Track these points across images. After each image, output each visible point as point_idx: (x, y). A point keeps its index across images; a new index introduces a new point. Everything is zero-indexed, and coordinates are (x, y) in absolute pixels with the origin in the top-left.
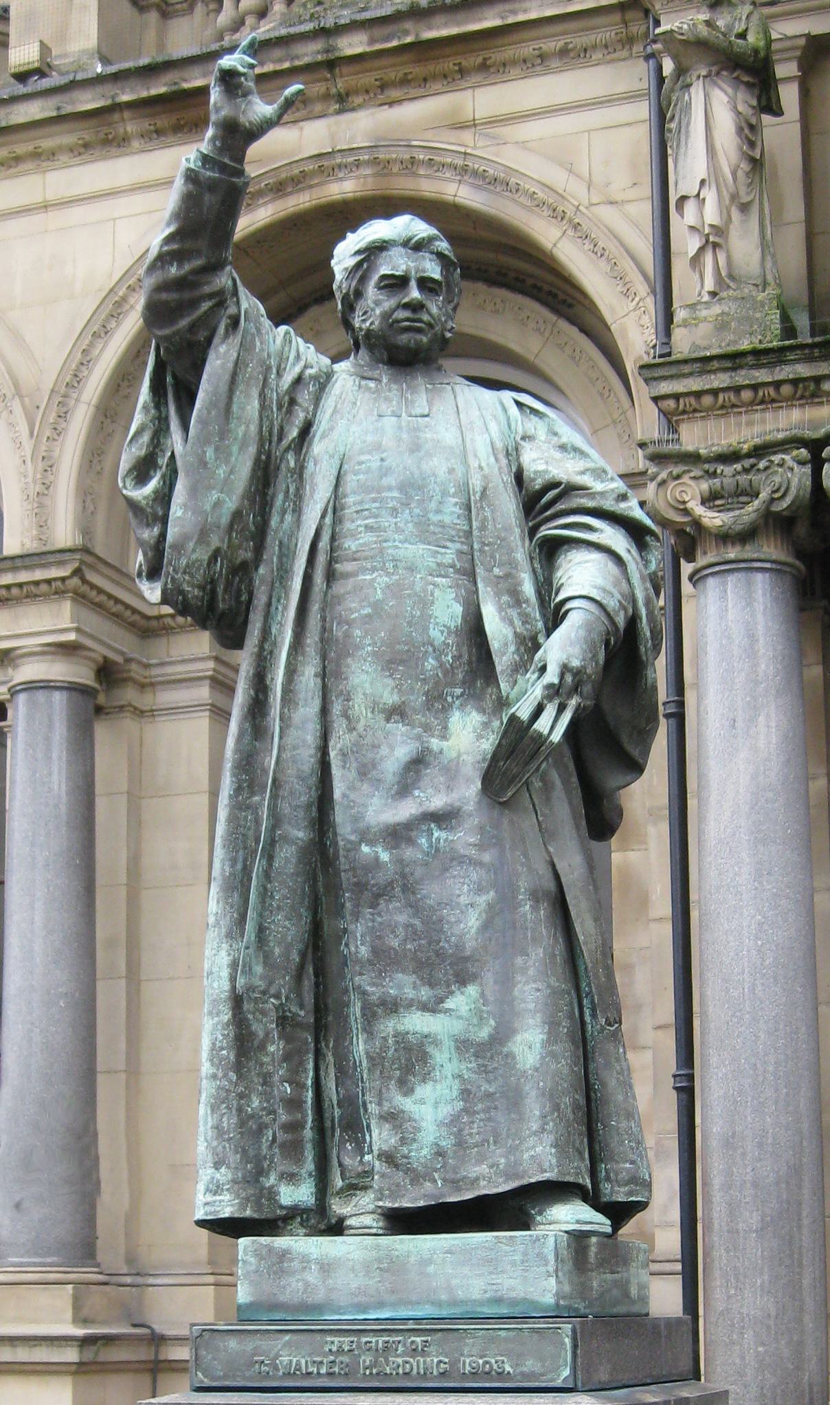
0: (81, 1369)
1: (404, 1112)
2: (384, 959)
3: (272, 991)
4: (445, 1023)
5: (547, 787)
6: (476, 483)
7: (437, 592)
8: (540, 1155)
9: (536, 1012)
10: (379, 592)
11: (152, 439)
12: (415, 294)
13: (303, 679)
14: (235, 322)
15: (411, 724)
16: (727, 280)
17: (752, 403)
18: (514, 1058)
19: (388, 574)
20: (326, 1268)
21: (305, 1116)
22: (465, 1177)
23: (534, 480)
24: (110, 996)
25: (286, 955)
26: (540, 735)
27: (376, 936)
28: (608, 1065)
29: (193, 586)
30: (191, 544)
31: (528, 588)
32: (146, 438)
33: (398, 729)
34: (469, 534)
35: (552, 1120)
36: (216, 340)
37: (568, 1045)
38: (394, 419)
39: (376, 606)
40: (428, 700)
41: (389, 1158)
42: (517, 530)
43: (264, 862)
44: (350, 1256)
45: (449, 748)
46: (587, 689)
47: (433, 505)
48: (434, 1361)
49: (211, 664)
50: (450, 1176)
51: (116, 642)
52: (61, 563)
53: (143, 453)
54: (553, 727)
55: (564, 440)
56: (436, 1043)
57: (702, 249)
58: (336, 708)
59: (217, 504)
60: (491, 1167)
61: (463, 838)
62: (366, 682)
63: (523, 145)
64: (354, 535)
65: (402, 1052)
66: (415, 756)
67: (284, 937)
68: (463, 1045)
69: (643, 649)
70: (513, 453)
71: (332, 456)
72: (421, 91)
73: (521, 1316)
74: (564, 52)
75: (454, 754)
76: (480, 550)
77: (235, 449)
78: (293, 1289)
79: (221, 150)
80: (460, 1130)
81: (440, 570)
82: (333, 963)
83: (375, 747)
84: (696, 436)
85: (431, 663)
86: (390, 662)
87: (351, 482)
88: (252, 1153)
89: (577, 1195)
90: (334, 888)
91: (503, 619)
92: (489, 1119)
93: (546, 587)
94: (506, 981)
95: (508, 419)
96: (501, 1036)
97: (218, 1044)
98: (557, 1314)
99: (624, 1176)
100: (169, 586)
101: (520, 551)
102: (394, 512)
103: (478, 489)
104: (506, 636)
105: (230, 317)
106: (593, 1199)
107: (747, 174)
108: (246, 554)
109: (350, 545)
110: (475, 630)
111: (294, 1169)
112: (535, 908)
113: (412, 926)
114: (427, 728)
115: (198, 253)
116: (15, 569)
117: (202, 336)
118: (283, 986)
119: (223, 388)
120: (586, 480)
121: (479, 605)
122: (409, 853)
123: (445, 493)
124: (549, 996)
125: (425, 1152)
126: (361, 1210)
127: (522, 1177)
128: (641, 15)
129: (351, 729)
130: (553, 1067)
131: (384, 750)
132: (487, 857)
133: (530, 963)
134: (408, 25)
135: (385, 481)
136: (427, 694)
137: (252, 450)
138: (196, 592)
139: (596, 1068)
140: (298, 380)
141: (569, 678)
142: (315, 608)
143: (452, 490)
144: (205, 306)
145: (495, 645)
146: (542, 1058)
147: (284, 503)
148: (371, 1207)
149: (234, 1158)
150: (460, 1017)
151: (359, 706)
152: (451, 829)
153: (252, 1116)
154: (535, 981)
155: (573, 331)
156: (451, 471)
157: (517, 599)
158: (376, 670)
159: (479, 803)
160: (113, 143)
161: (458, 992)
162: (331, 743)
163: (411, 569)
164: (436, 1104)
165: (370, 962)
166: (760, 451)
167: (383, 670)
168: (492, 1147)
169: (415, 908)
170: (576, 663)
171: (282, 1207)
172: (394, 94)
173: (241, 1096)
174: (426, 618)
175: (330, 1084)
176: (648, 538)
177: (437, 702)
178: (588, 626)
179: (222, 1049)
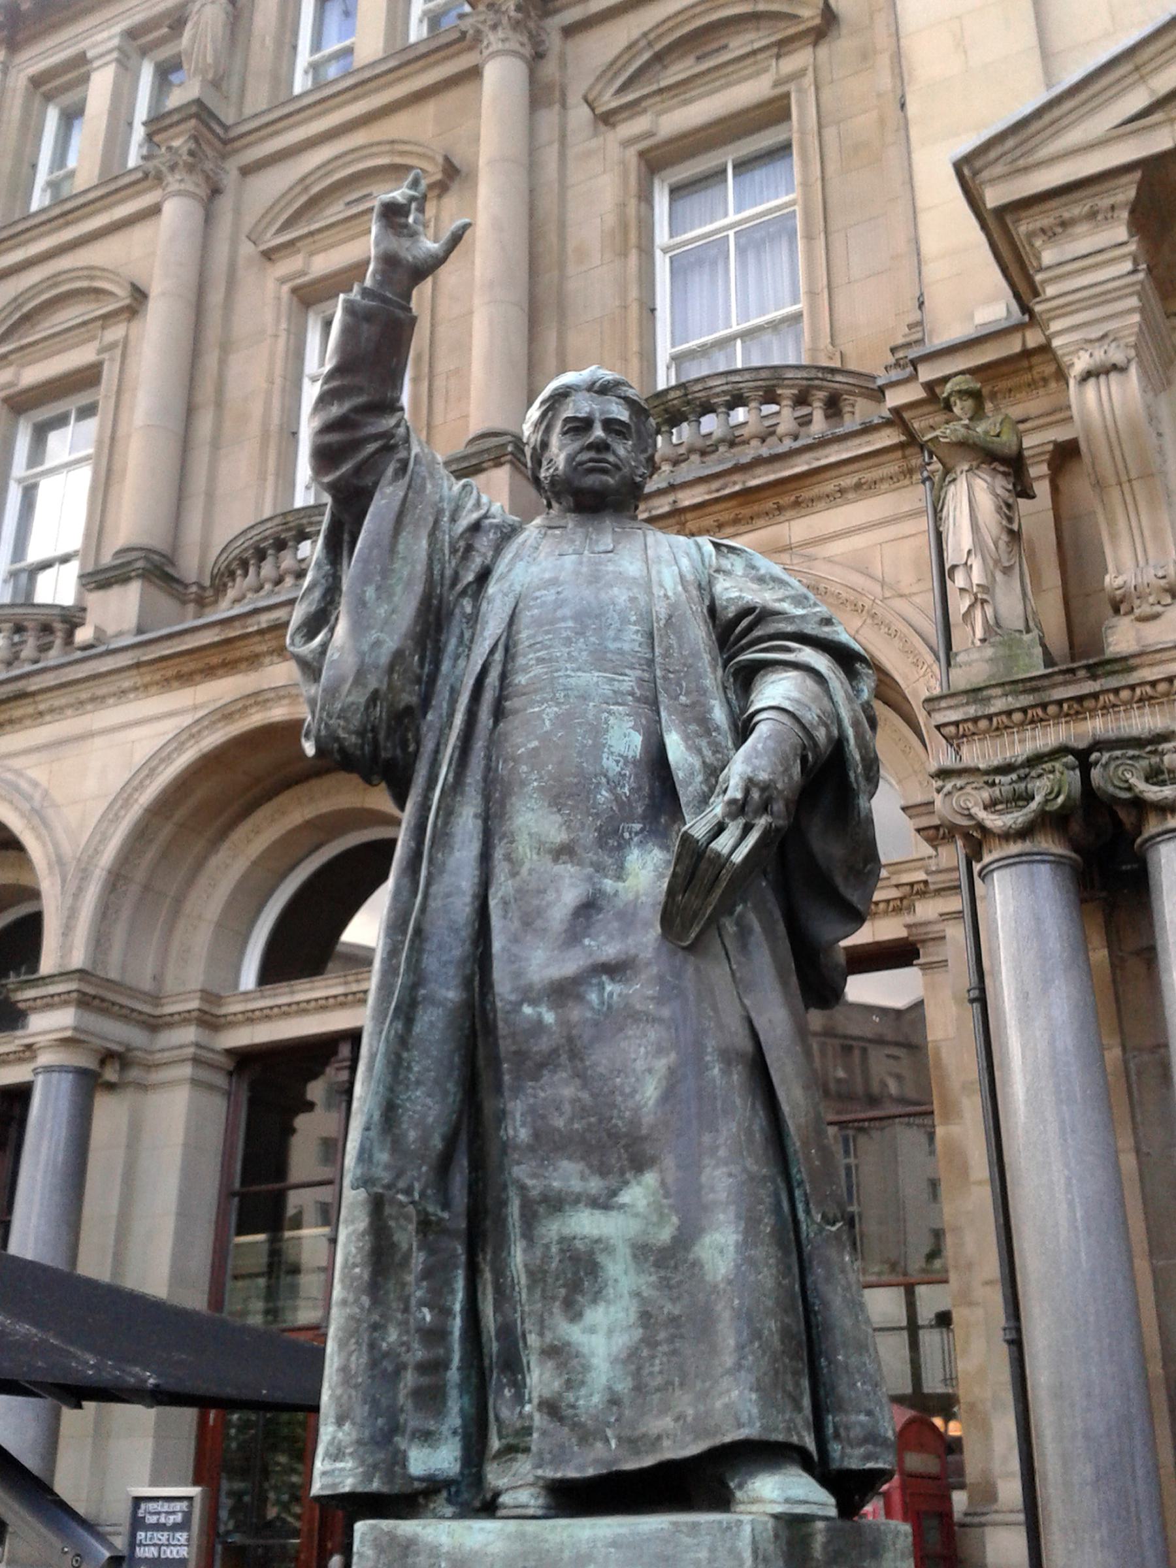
1: (569, 1344)
2: (548, 1144)
3: (402, 1184)
4: (616, 1223)
5: (744, 931)
6: (661, 609)
7: (612, 721)
8: (732, 1402)
9: (728, 1204)
10: (547, 723)
11: (324, 596)
13: (461, 821)
15: (580, 863)
16: (994, 628)
17: (1022, 724)
18: (702, 1267)
19: (558, 704)
21: (449, 1351)
22: (644, 1435)
23: (726, 608)
25: (425, 1139)
26: (719, 855)
27: (535, 1114)
28: (829, 1278)
29: (350, 733)
30: (347, 686)
32: (317, 594)
33: (567, 870)
34: (651, 662)
35: (753, 1353)
36: (383, 482)
37: (773, 1250)
38: (574, 557)
39: (545, 738)
40: (600, 838)
41: (551, 1408)
42: (707, 657)
43: (399, 1025)
44: (490, 1549)
45: (626, 890)
46: (778, 806)
47: (611, 633)
50: (627, 1432)
53: (313, 608)
55: (762, 571)
56: (609, 1250)
57: (972, 606)
58: (498, 854)
59: (377, 644)
60: (677, 1419)
62: (533, 822)
63: (829, 560)
64: (525, 669)
65: (568, 1263)
66: (585, 900)
67: (424, 1116)
68: (642, 1252)
69: (852, 775)
70: (705, 588)
71: (506, 595)
72: (749, 527)
74: (858, 486)
75: (631, 896)
76: (665, 678)
77: (399, 589)
79: (381, 284)
80: (639, 1369)
81: (617, 698)
83: (541, 892)
84: (976, 754)
85: (604, 795)
86: (558, 796)
87: (525, 617)
88: (384, 1402)
89: (792, 1461)
91: (688, 748)
92: (674, 1352)
94: (691, 1167)
95: (702, 555)
96: (685, 1239)
97: (351, 1260)
99: (856, 1432)
100: (323, 733)
101: (711, 677)
102: (568, 642)
103: (663, 616)
104: (692, 765)
105: (399, 461)
107: (1007, 544)
108: (409, 698)
109: (521, 679)
110: (657, 761)
111: (431, 1425)
112: (726, 1072)
113: (579, 1100)
114: (599, 868)
115: (360, 390)
117: (368, 481)
118: (418, 1179)
119: (388, 525)
120: (786, 606)
121: (662, 736)
122: (576, 1013)
123: (625, 621)
124: (744, 1183)
125: (596, 1399)
127: (715, 1435)
128: (917, 450)
129: (514, 874)
130: (752, 1278)
131: (551, 896)
132: (666, 1012)
133: (721, 1140)
134: (735, 478)
135: (559, 614)
136: (599, 830)
137: (419, 588)
138: (353, 739)
139: (815, 1283)
140: (476, 527)
141: (755, 795)
142: (479, 745)
143: (634, 618)
144: (371, 447)
145: (679, 775)
146: (738, 1267)
147: (457, 647)
148: (530, 1478)
149: (361, 1411)
150: (636, 1215)
151: (524, 848)
152: (627, 981)
153: (386, 1355)
154: (726, 1164)
156: (633, 600)
158: (541, 807)
159: (658, 950)
161: (634, 1183)
162: (492, 891)
163: (584, 697)
164: (610, 1332)
165: (531, 1148)
166: (1035, 760)
167: (550, 806)
168: (678, 1393)
169: (582, 1077)
170: (763, 776)
171: (413, 1479)
173: (375, 1327)
174: (598, 748)
175: (488, 1309)
176: (858, 665)
177: (611, 840)
179: (355, 1265)
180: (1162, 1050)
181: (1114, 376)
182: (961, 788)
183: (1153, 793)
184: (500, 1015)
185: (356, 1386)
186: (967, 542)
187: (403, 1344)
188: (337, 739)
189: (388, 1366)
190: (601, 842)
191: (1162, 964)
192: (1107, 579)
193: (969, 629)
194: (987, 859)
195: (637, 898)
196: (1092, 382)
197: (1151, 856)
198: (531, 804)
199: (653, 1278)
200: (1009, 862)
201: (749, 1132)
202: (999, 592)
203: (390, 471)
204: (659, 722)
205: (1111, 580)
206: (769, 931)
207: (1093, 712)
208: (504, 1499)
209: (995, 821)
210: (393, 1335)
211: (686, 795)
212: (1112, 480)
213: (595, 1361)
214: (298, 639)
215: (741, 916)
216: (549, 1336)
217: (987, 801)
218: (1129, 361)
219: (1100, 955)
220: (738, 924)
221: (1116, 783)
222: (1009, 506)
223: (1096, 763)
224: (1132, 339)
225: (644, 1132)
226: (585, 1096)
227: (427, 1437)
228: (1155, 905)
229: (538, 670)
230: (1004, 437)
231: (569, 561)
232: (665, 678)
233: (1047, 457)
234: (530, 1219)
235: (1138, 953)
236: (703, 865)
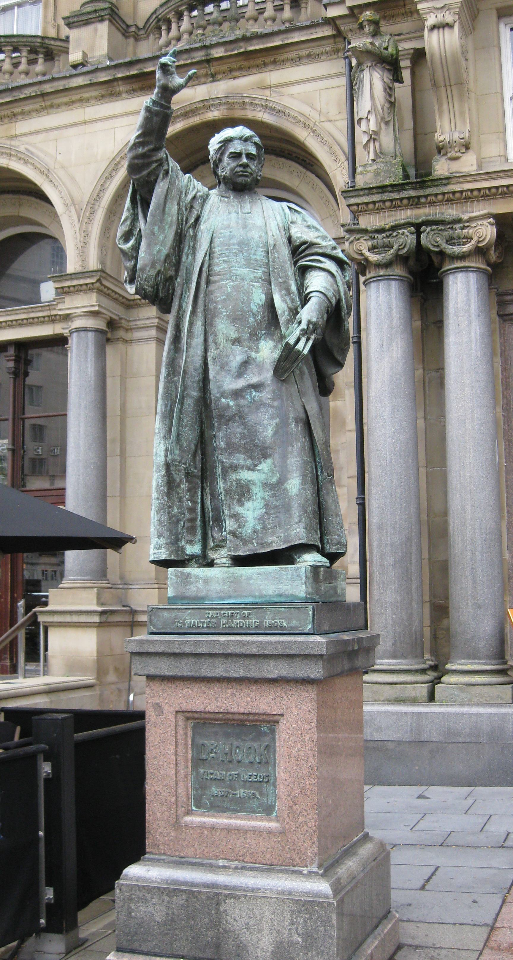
0: (100, 625)
2: (231, 448)
3: (183, 462)
4: (258, 475)
5: (302, 373)
6: (271, 242)
8: (299, 533)
11: (131, 223)
12: (244, 160)
13: (197, 327)
14: (167, 172)
15: (243, 346)
16: (379, 154)
17: (390, 207)
18: (287, 490)
19: (233, 281)
20: (206, 581)
21: (197, 515)
23: (296, 241)
24: (113, 464)
26: (299, 351)
28: (328, 493)
29: (149, 287)
30: (148, 268)
32: (128, 223)
34: (268, 264)
36: (159, 180)
39: (228, 295)
40: (250, 336)
41: (233, 533)
42: (289, 263)
43: (179, 406)
46: (319, 331)
47: (252, 252)
48: (253, 621)
51: (115, 311)
52: (92, 277)
53: (127, 229)
54: (304, 347)
55: (309, 223)
56: (254, 484)
57: (368, 141)
58: (211, 339)
59: (159, 251)
61: (265, 395)
62: (224, 328)
67: (188, 438)
68: (265, 485)
69: (343, 314)
71: (209, 230)
73: (290, 602)
74: (309, 56)
75: (261, 359)
76: (273, 271)
77: (167, 227)
78: (192, 590)
79: (161, 98)
80: (264, 522)
82: (209, 449)
83: (227, 356)
85: (251, 320)
86: (234, 319)
87: (217, 241)
88: (174, 531)
90: (210, 417)
91: (283, 301)
92: (277, 517)
93: (301, 287)
94: (284, 457)
95: (285, 214)
96: (282, 481)
98: (306, 601)
101: (290, 271)
102: (236, 254)
103: (272, 244)
105: (165, 170)
106: (321, 551)
107: (388, 108)
108: (171, 273)
109: (217, 269)
110: (270, 305)
112: (296, 426)
113: (243, 433)
114: (250, 348)
116: (72, 279)
120: (319, 241)
122: (242, 402)
125: (249, 531)
126: (221, 556)
128: (342, 40)
129: (217, 348)
130: (304, 494)
131: (231, 358)
132: (276, 404)
135: (232, 241)
136: (250, 333)
138: (150, 289)
140: (194, 198)
141: (311, 326)
144: (154, 165)
145: (279, 312)
146: (300, 490)
149: (167, 534)
150: (264, 473)
151: (220, 338)
152: (260, 391)
153: (174, 516)
156: (260, 237)
157: (289, 292)
159: (272, 380)
160: (114, 95)
162: (208, 354)
163: (243, 279)
165: (225, 449)
166: (394, 228)
169: (245, 426)
170: (314, 320)
172: (236, 74)
173: (170, 507)
174: (249, 300)
175: (208, 502)
176: (345, 266)
177: (254, 337)
178: (319, 304)
179: (161, 486)
180: (441, 371)
181: (447, 30)
182: (358, 239)
183: (450, 249)
184: (213, 402)
185: (164, 526)
187: (179, 512)
188: (144, 289)
189: (174, 519)
190: (250, 338)
191: (445, 333)
192: (436, 136)
193: (366, 153)
194: (368, 276)
195: (264, 360)
196: (436, 31)
197: (445, 280)
198: (224, 321)
199: (270, 493)
200: (379, 279)
201: (304, 446)
203: (161, 176)
204: (271, 289)
205: (438, 137)
206: (310, 371)
207: (424, 205)
208: (216, 561)
209: (373, 258)
211: (282, 319)
212: (443, 85)
213: (248, 519)
214: (121, 241)
215: (301, 367)
216: (232, 511)
217: (371, 247)
218: (455, 22)
220: (300, 370)
221: (433, 243)
222: (390, 88)
223: (424, 232)
224: (457, 10)
225: (267, 445)
226: (245, 432)
227: (191, 542)
228: (445, 304)
230: (390, 50)
231: (234, 215)
232: (273, 271)
233: (410, 56)
234: (225, 473)
235: (435, 323)
236: (293, 353)
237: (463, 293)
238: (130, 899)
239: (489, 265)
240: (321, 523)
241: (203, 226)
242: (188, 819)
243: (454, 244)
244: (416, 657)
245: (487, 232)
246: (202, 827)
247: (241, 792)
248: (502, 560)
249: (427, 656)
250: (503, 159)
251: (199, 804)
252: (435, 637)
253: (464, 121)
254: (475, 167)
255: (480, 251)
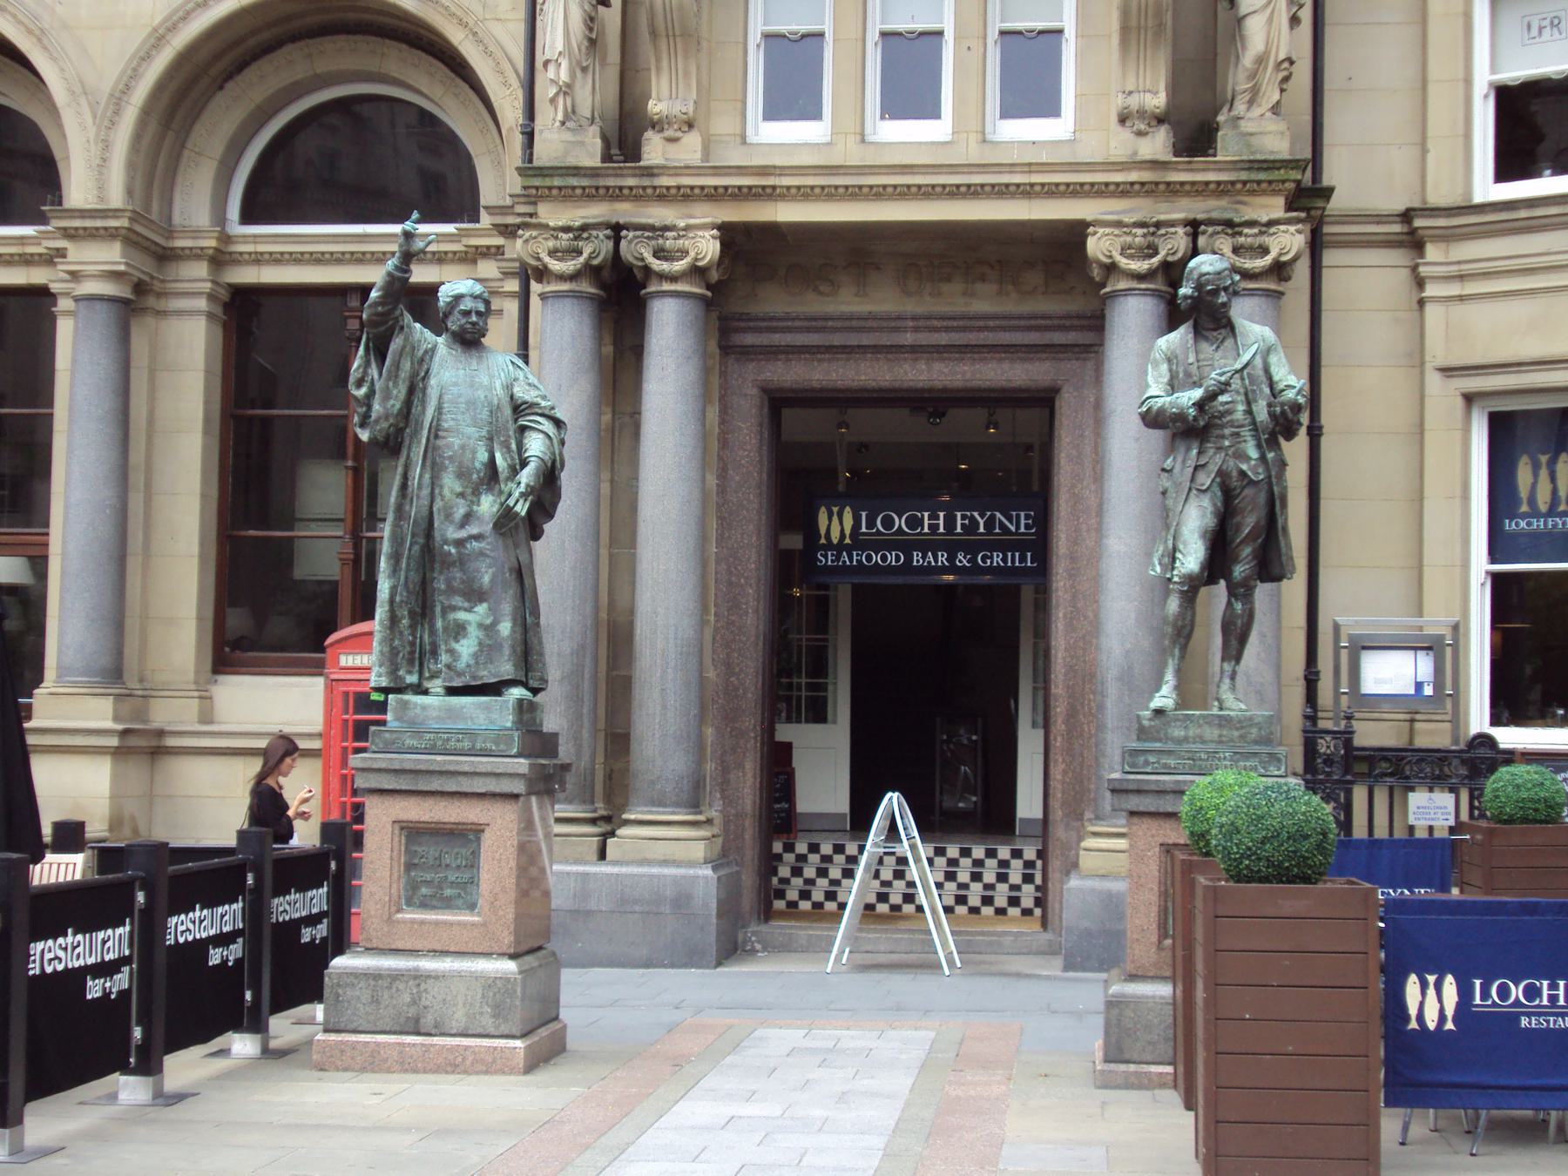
0: (118, 753)
2: (451, 590)
8: (506, 669)
12: (474, 319)
14: (402, 328)
20: (424, 708)
31: (514, 446)
41: (449, 667)
48: (466, 744)
49: (209, 285)
51: (146, 265)
54: (522, 509)
57: (557, 94)
62: (450, 483)
68: (480, 626)
82: (429, 590)
87: (446, 398)
90: (432, 561)
93: (520, 445)
96: (495, 623)
101: (512, 428)
106: (525, 685)
110: (492, 461)
116: (83, 217)
120: (539, 400)
126: (436, 686)
151: (446, 492)
155: (465, 87)
157: (509, 449)
166: (584, 228)
169: (464, 571)
174: (474, 459)
177: (476, 493)
178: (537, 469)
183: (657, 265)
186: (560, 47)
202: (578, 85)
210: (396, 642)
219: (609, 349)
227: (410, 672)
229: (452, 423)
237: (670, 329)
238: (339, 985)
239: (709, 287)
240: (526, 661)
241: (433, 382)
242: (400, 916)
243: (666, 259)
244: (584, 802)
245: (707, 247)
246: (413, 921)
247: (448, 892)
248: (702, 681)
249: (600, 805)
250: (738, 139)
251: (409, 903)
252: (609, 777)
253: (688, 85)
254: (698, 155)
255: (697, 272)
